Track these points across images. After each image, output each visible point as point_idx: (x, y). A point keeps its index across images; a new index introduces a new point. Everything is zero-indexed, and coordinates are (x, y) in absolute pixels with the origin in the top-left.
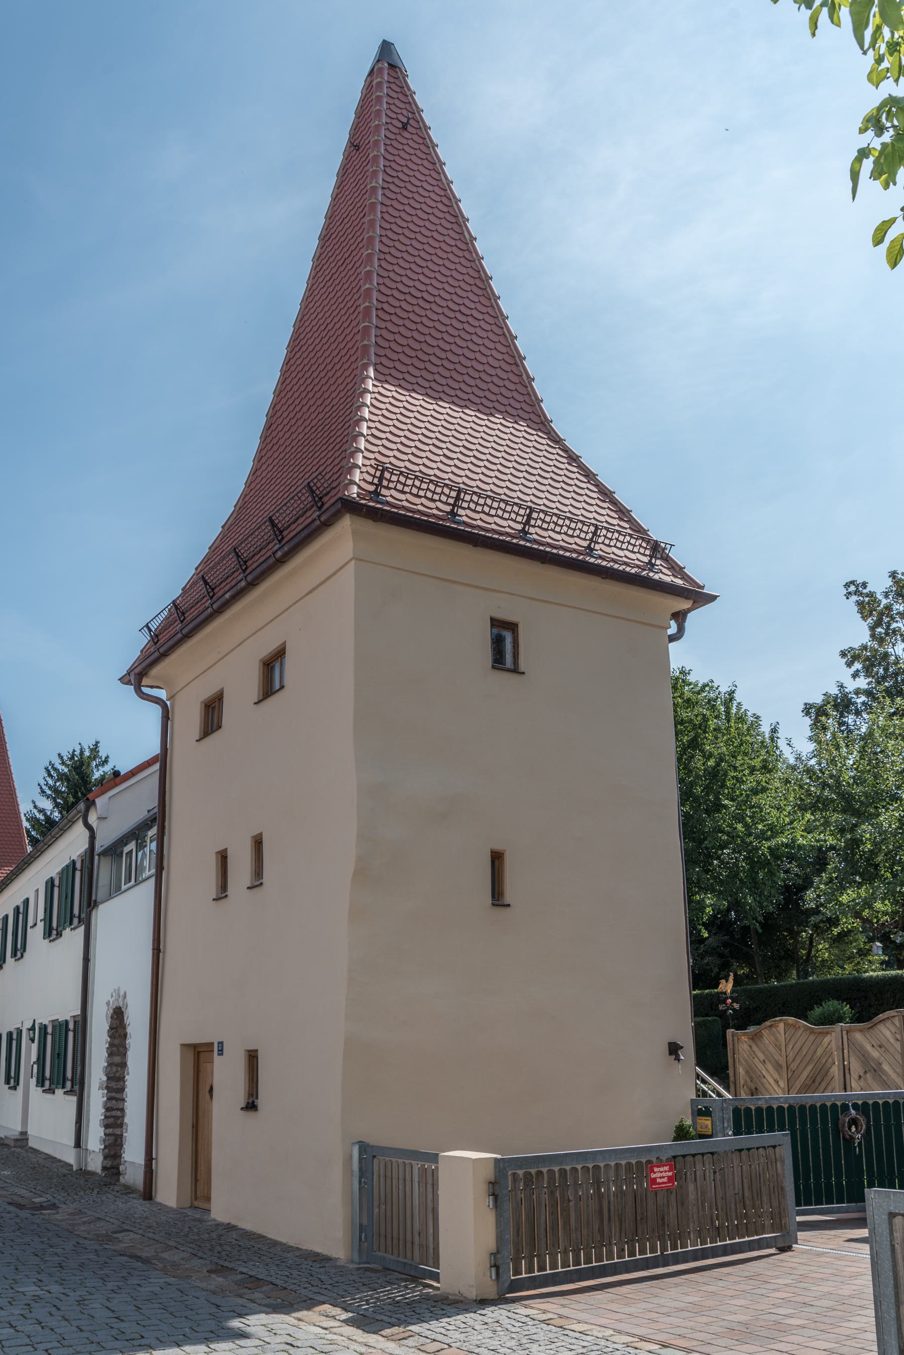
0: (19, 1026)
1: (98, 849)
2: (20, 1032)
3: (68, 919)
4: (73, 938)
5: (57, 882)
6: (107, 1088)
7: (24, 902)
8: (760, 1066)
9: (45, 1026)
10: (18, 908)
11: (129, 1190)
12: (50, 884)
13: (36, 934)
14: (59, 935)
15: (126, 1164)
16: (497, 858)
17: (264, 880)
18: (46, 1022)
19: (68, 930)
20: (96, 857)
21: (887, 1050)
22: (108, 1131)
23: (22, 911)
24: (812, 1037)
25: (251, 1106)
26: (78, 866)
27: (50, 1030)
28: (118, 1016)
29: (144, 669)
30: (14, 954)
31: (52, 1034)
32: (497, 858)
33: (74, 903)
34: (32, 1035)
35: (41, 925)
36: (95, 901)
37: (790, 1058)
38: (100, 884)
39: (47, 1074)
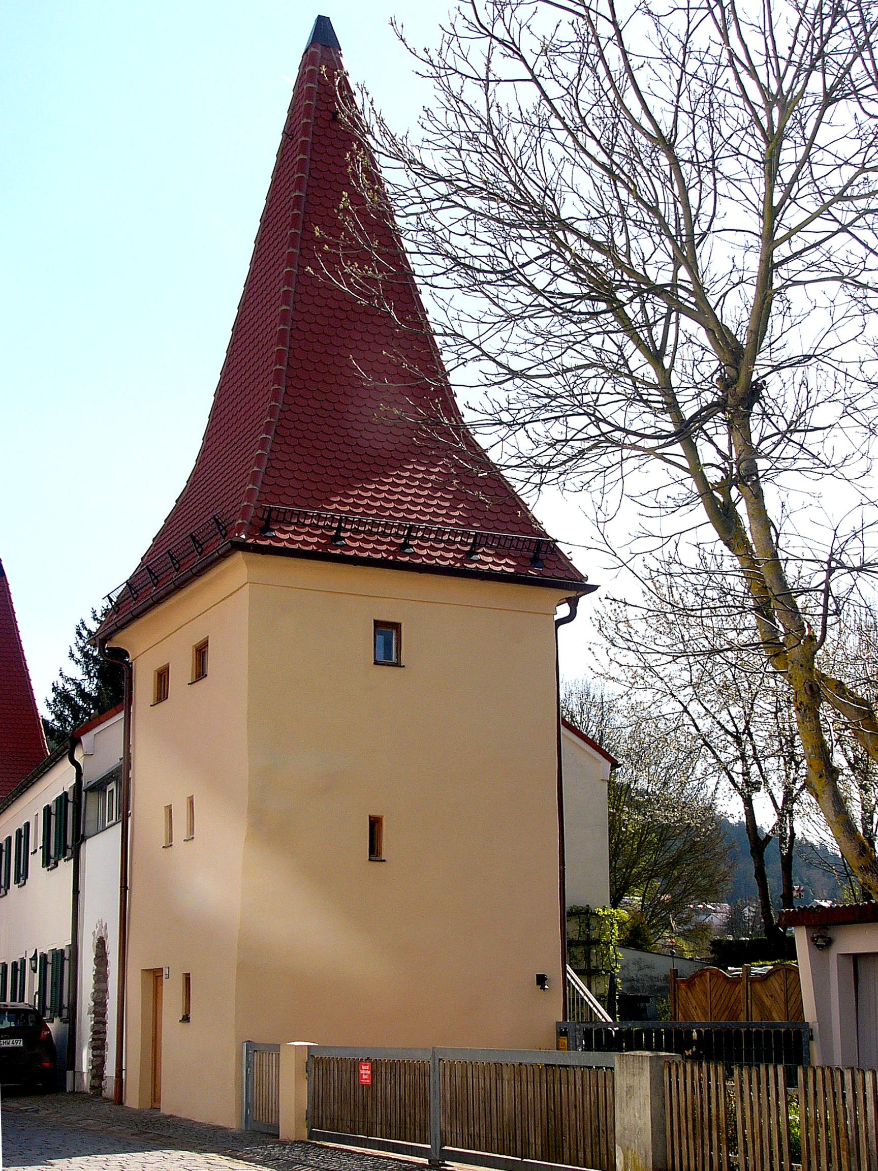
0: (23, 956)
1: (84, 785)
2: (23, 961)
3: (62, 851)
4: (66, 867)
5: (53, 810)
6: (94, 1012)
7: (6, 840)
8: (693, 1011)
9: (45, 955)
10: (19, 831)
11: (107, 1100)
12: (47, 810)
13: (36, 861)
14: (56, 864)
15: (107, 1079)
16: (375, 824)
17: (195, 836)
18: (46, 952)
19: (63, 860)
20: (84, 793)
21: (775, 999)
22: (95, 1053)
23: (23, 835)
24: (728, 987)
25: (186, 1019)
26: (70, 797)
27: (50, 959)
28: (101, 944)
29: (107, 636)
30: (17, 881)
31: (52, 964)
32: (375, 824)
33: (66, 835)
34: (34, 965)
35: (40, 852)
36: (83, 835)
37: (713, 1005)
38: (87, 819)
39: (48, 1004)
